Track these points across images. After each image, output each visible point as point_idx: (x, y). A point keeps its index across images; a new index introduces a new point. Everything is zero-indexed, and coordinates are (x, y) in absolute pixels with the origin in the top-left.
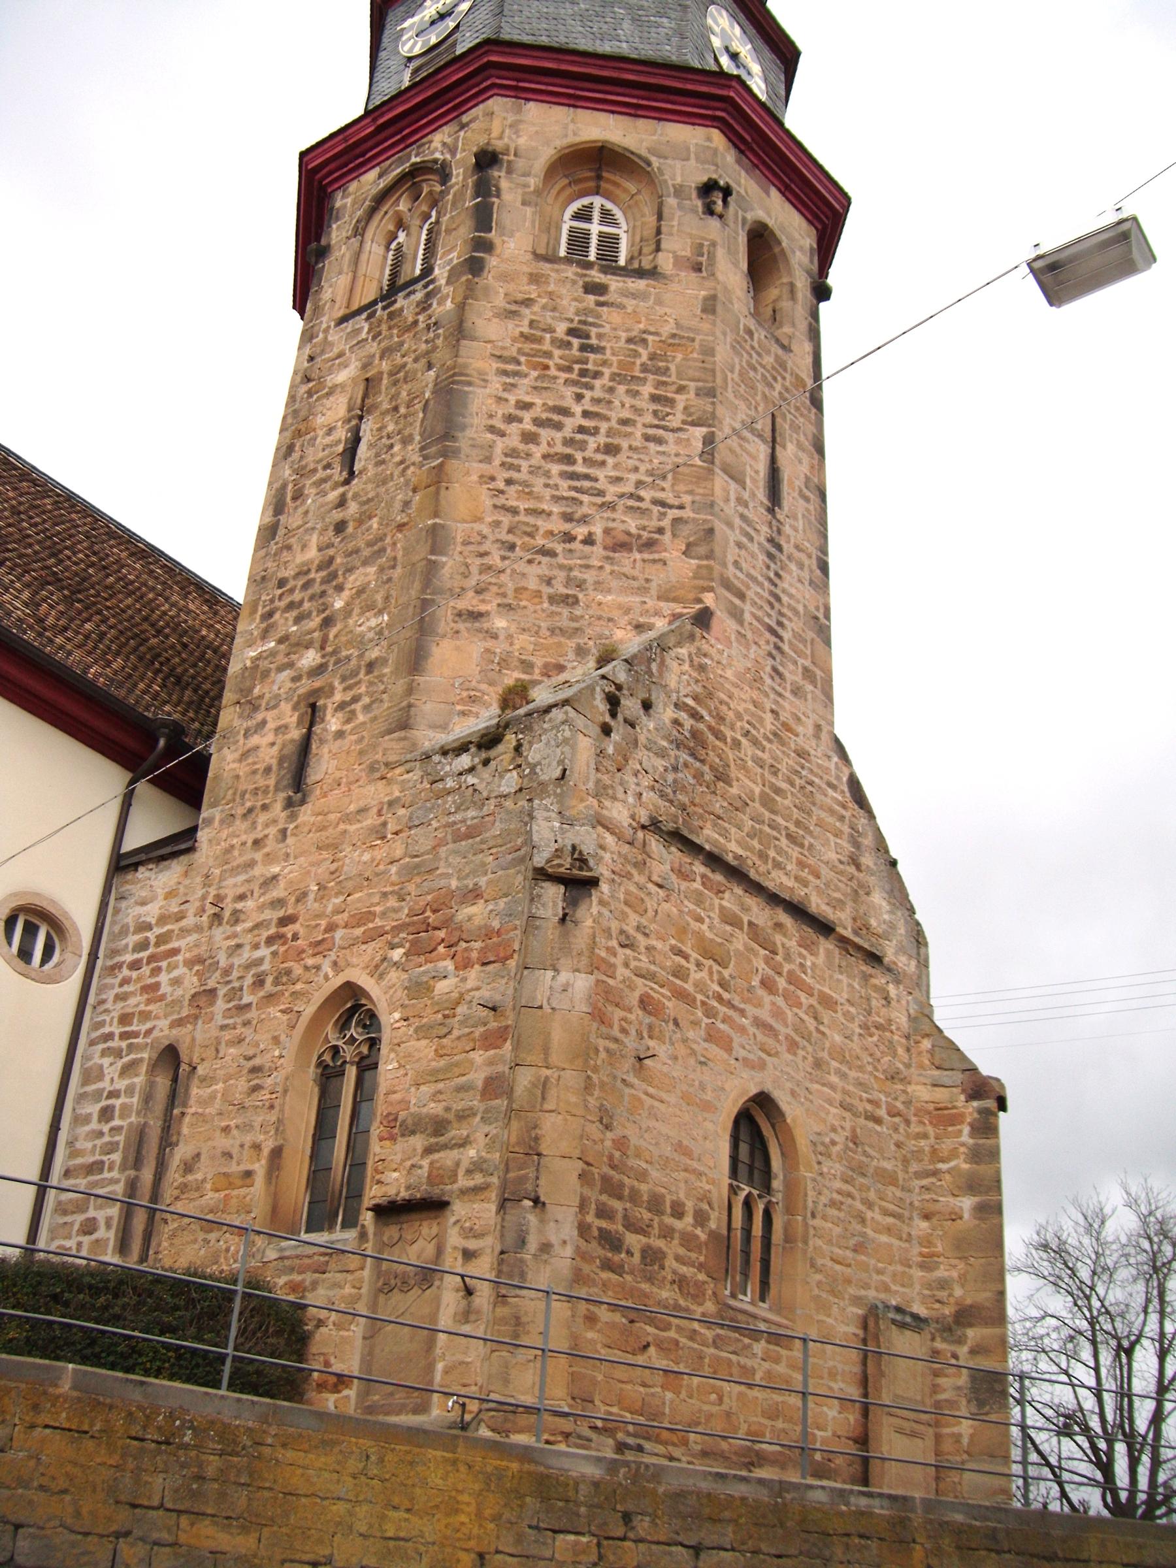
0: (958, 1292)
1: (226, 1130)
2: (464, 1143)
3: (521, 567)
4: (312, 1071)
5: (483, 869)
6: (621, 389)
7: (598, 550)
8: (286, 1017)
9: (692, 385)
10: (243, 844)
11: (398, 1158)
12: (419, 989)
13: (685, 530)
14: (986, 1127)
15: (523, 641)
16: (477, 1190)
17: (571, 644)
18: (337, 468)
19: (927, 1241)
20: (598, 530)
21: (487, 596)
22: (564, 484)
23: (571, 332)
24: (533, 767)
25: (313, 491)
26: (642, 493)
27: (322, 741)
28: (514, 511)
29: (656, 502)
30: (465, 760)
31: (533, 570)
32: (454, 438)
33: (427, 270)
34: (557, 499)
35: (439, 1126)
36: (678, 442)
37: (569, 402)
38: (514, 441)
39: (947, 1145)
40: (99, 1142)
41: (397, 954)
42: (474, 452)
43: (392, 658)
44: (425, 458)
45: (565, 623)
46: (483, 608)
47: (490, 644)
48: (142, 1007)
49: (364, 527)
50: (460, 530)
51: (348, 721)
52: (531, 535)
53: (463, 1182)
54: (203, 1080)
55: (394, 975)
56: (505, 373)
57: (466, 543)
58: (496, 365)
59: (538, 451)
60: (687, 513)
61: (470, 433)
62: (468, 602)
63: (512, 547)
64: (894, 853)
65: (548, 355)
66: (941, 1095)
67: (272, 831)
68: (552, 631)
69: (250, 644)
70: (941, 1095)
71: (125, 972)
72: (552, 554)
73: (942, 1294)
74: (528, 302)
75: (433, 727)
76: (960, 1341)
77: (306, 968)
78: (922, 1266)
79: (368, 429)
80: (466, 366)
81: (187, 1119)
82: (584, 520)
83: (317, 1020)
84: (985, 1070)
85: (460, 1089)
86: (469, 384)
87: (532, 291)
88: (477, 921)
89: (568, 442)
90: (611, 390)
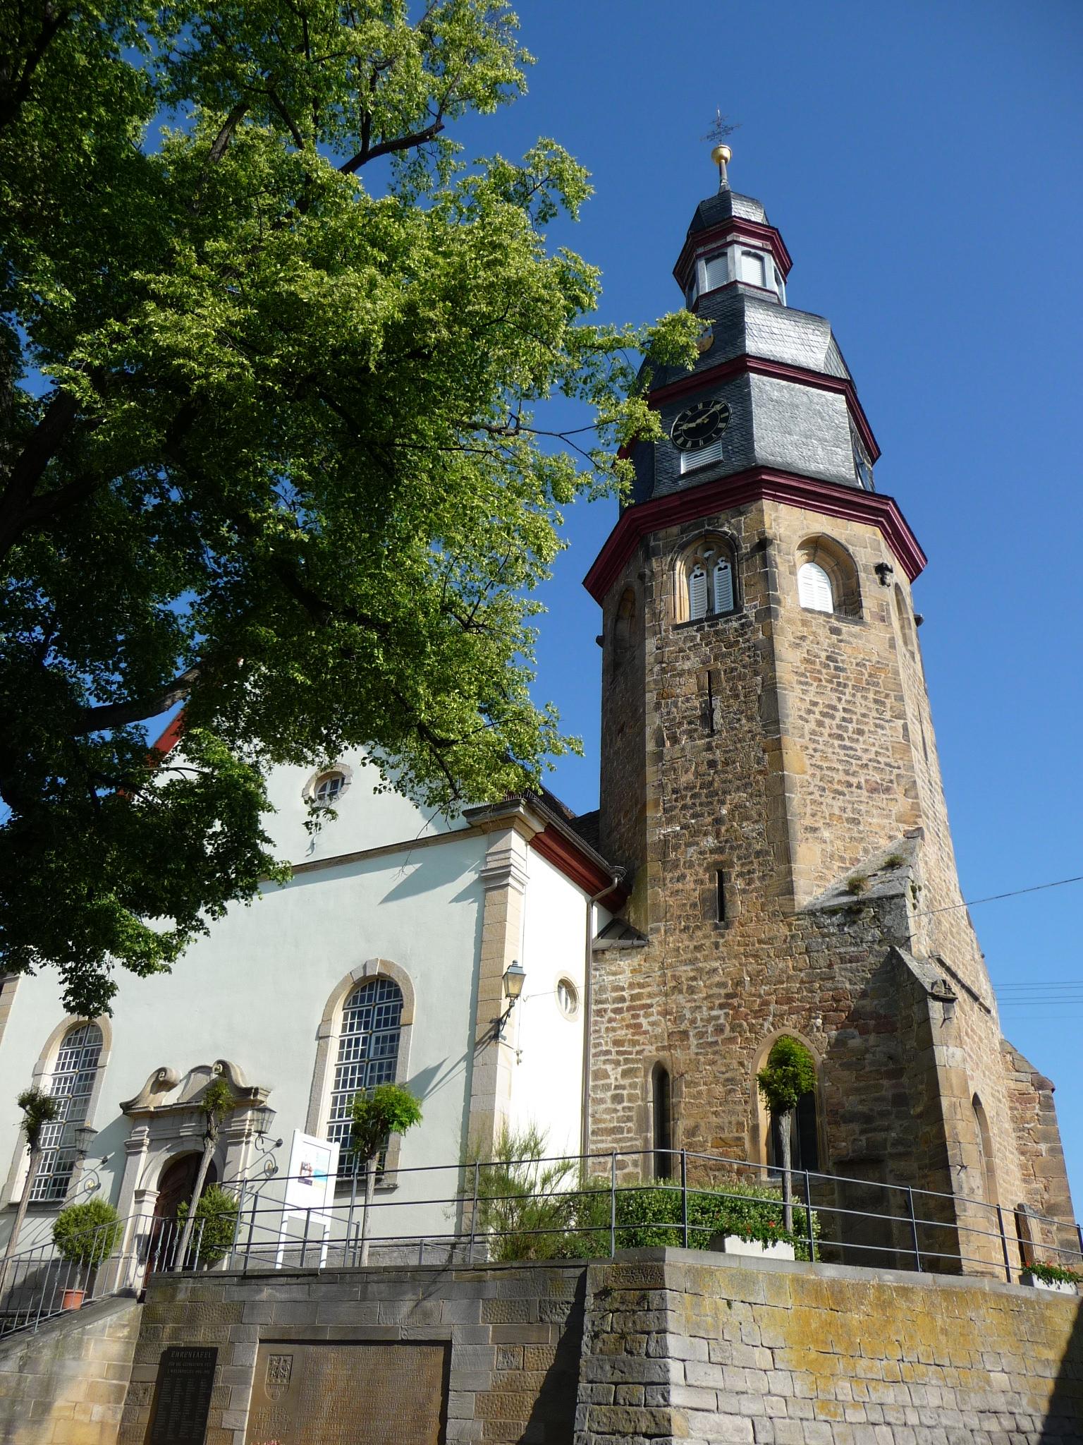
2: (888, 1129)
3: (830, 801)
6: (859, 695)
9: (892, 693)
11: (844, 1135)
13: (903, 781)
14: (1048, 1105)
21: (817, 818)
22: (842, 752)
23: (828, 658)
24: (889, 928)
28: (821, 768)
29: (887, 764)
33: (738, 608)
34: (840, 761)
35: (867, 1119)
36: (891, 728)
37: (835, 702)
38: (813, 725)
39: (1029, 1114)
42: (796, 731)
46: (816, 825)
47: (824, 846)
48: (630, 1037)
56: (801, 683)
59: (826, 731)
60: (902, 772)
61: (791, 719)
62: (808, 821)
63: (824, 790)
65: (819, 672)
66: (1020, 1086)
69: (659, 824)
70: (1020, 1086)
74: (803, 638)
75: (807, 893)
76: (1052, 1223)
79: (717, 703)
82: (854, 774)
84: (1043, 1074)
85: (877, 1099)
87: (805, 631)
88: (868, 1009)
89: (839, 727)
90: (854, 695)
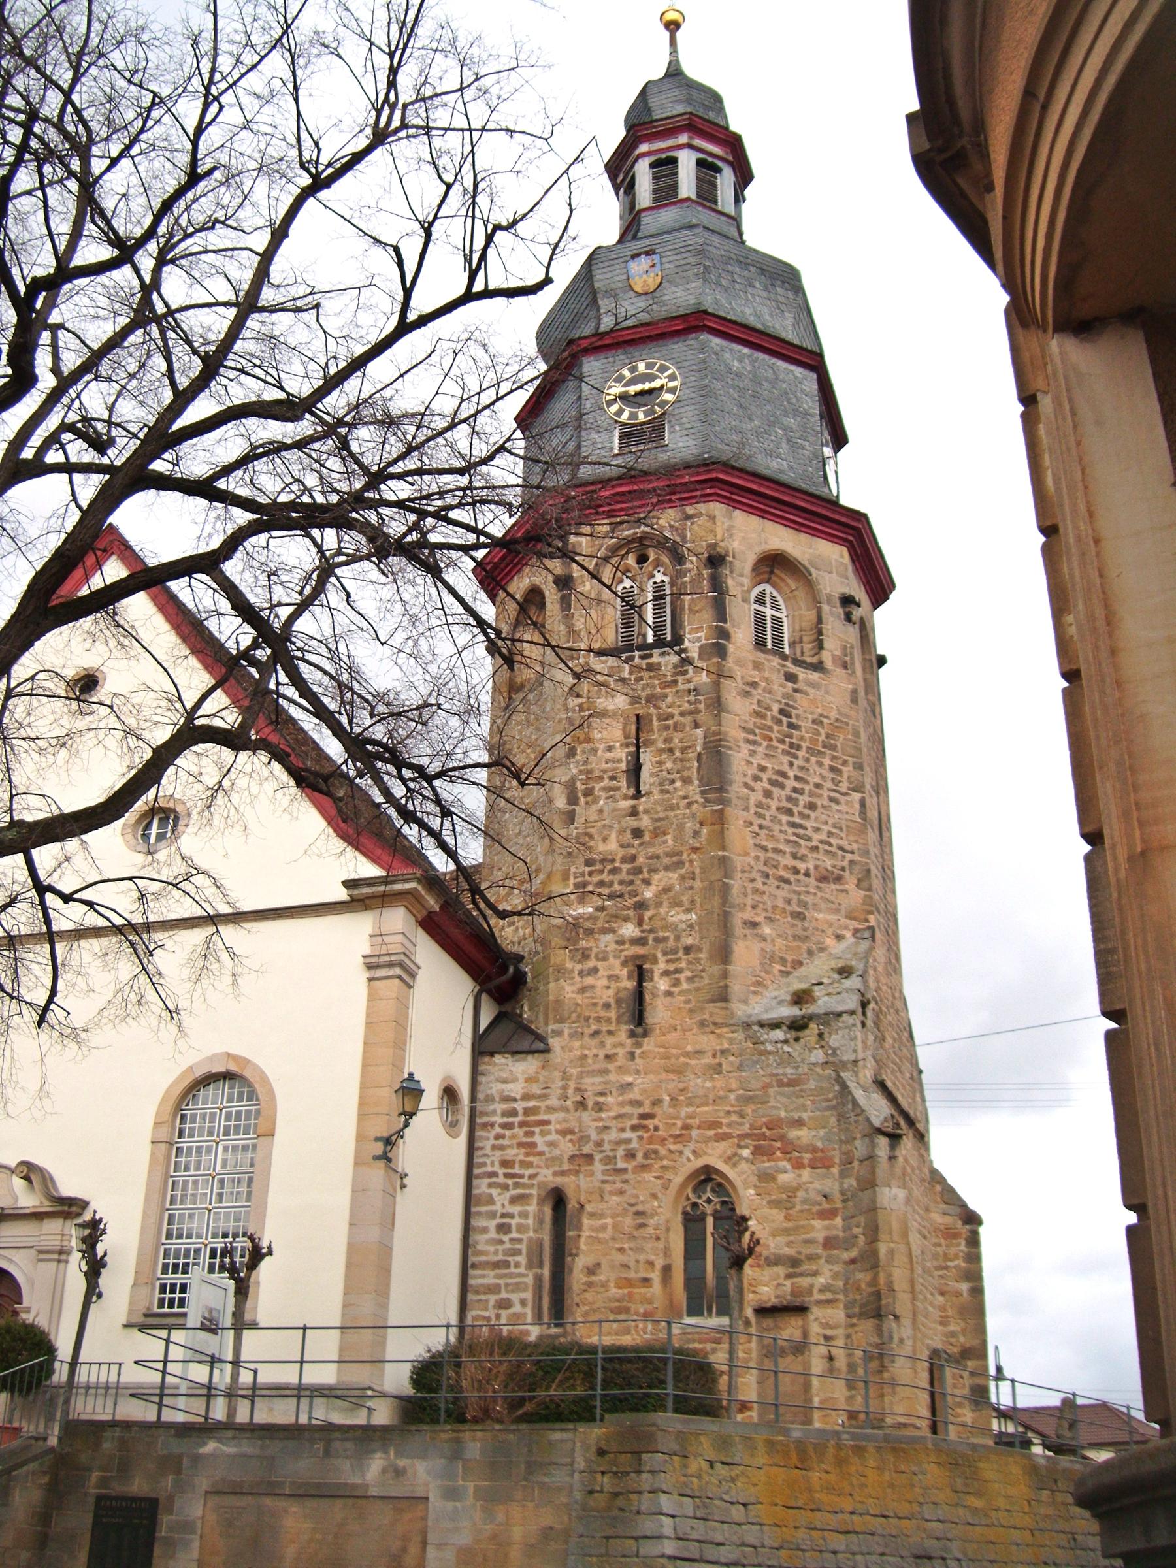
0: (962, 1339)
1: (621, 1250)
2: (815, 1274)
4: (680, 1217)
5: (804, 1108)
6: (813, 759)
7: (812, 881)
8: (659, 1182)
10: (596, 1056)
12: (766, 1177)
13: (857, 868)
15: (780, 942)
16: (829, 1302)
17: (804, 947)
18: (623, 783)
19: (942, 1308)
20: (811, 866)
22: (790, 830)
24: (834, 1050)
25: (603, 795)
26: (832, 840)
27: (654, 995)
28: (765, 849)
30: (779, 1034)
31: (780, 893)
32: (727, 791)
34: (788, 841)
35: (794, 1262)
37: (786, 768)
39: (952, 1251)
40: (500, 1247)
41: (746, 1153)
43: (706, 946)
44: (707, 801)
45: (800, 933)
47: (763, 945)
49: (659, 839)
50: (738, 861)
51: (674, 985)
52: (776, 867)
53: (817, 1296)
54: (592, 1215)
55: (743, 1165)
57: (743, 872)
58: (743, 735)
59: (774, 804)
60: (856, 857)
62: (748, 915)
63: (767, 876)
64: (921, 1066)
65: (770, 729)
67: (621, 1051)
68: (794, 936)
70: (948, 1220)
71: (498, 1130)
72: (787, 882)
73: (953, 1340)
77: (671, 1151)
78: (941, 1323)
79: (646, 757)
80: (726, 733)
81: (583, 1240)
82: (802, 858)
83: (683, 1186)
86: (730, 748)
90: (807, 760)
